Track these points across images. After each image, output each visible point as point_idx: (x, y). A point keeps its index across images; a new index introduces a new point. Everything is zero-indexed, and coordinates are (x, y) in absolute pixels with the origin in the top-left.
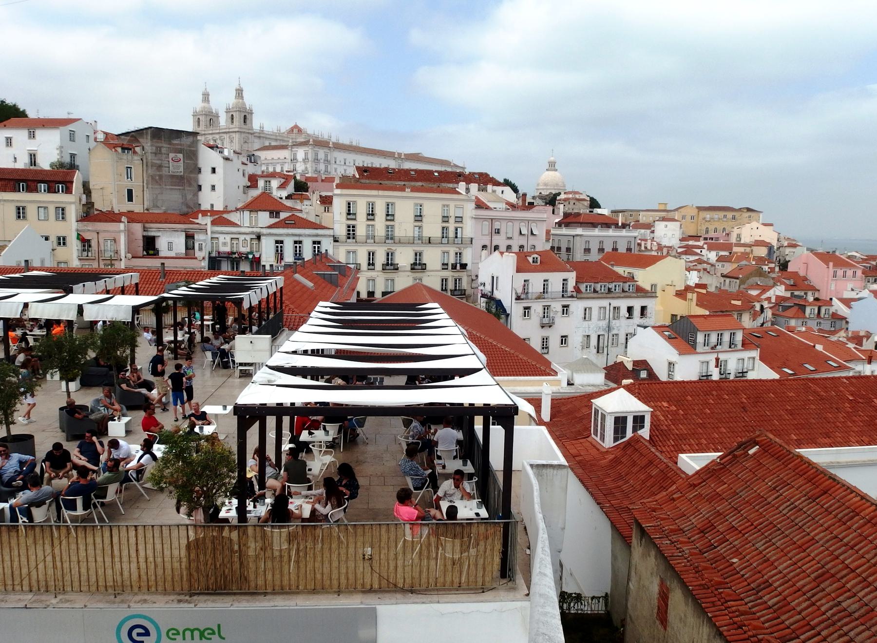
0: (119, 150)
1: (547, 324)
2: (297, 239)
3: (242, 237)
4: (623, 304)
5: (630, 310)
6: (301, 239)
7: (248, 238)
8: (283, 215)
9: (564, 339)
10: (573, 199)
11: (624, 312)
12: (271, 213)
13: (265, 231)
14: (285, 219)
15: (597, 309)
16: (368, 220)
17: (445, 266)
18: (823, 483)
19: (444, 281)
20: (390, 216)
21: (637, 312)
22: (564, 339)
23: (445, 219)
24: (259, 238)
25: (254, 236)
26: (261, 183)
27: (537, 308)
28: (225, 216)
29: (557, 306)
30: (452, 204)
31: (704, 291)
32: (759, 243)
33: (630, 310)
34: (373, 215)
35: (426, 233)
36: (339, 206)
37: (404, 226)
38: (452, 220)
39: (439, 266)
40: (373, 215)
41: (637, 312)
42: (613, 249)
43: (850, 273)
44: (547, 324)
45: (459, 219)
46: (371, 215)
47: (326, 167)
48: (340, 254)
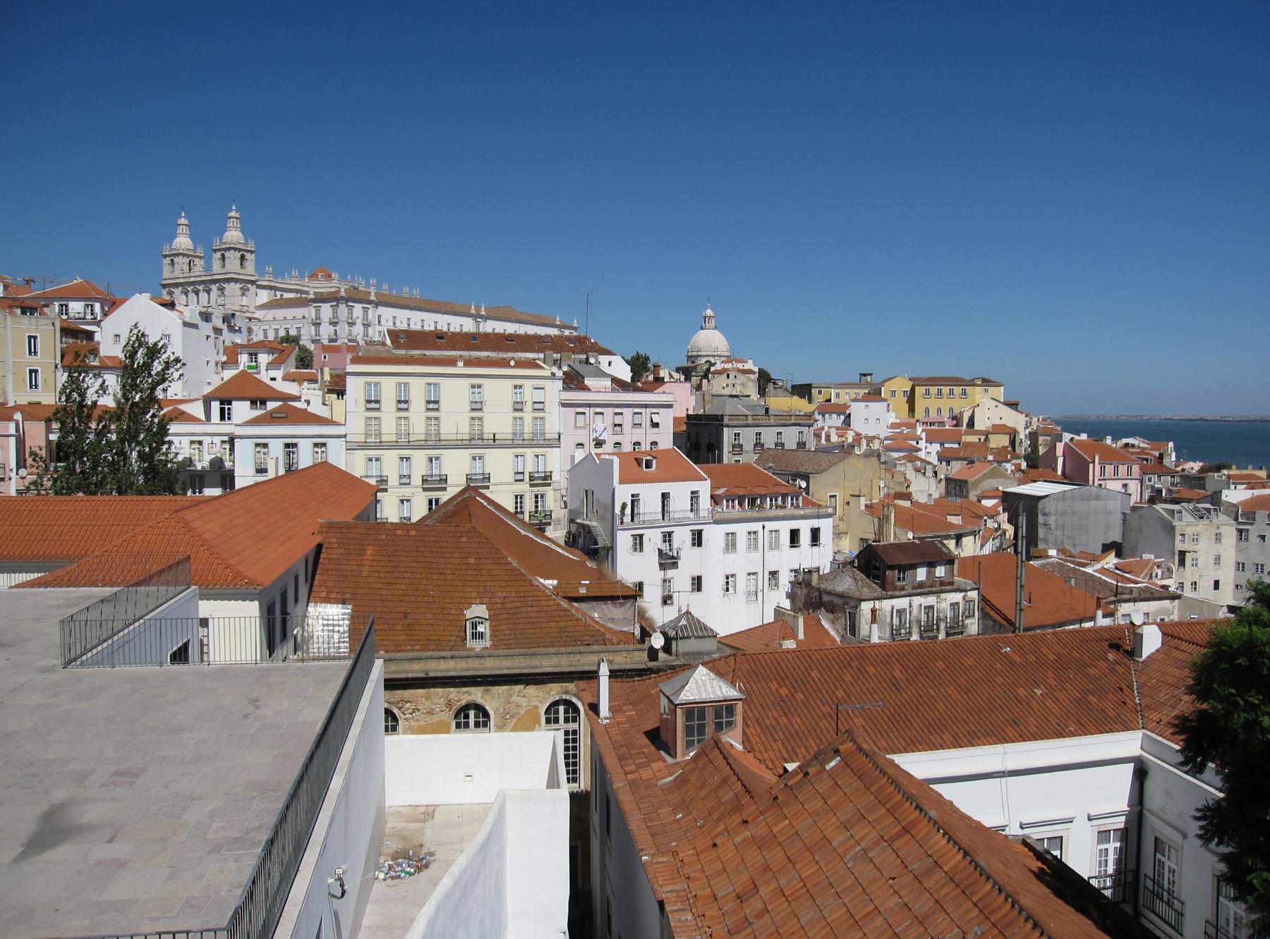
0: (19, 311)
1: (668, 561)
2: (289, 441)
3: (207, 440)
4: (785, 527)
5: (794, 535)
6: (294, 441)
7: (217, 440)
8: (271, 405)
9: (697, 583)
10: (734, 369)
11: (785, 538)
12: (253, 403)
13: (239, 431)
14: (273, 411)
15: (745, 534)
16: (399, 409)
17: (519, 477)
18: (919, 800)
19: (519, 498)
20: (433, 404)
21: (805, 537)
22: (697, 583)
23: (518, 407)
24: (231, 441)
25: (226, 438)
26: (244, 359)
27: (653, 539)
28: (183, 407)
29: (682, 537)
30: (528, 384)
31: (906, 504)
32: (999, 429)
33: (794, 535)
34: (437, 402)
35: (488, 430)
36: (354, 386)
37: (455, 422)
38: (528, 407)
39: (510, 477)
40: (406, 402)
41: (805, 537)
42: (776, 444)
43: (1123, 469)
44: (668, 561)
45: (539, 407)
46: (403, 403)
47: (318, 333)
48: (356, 465)
